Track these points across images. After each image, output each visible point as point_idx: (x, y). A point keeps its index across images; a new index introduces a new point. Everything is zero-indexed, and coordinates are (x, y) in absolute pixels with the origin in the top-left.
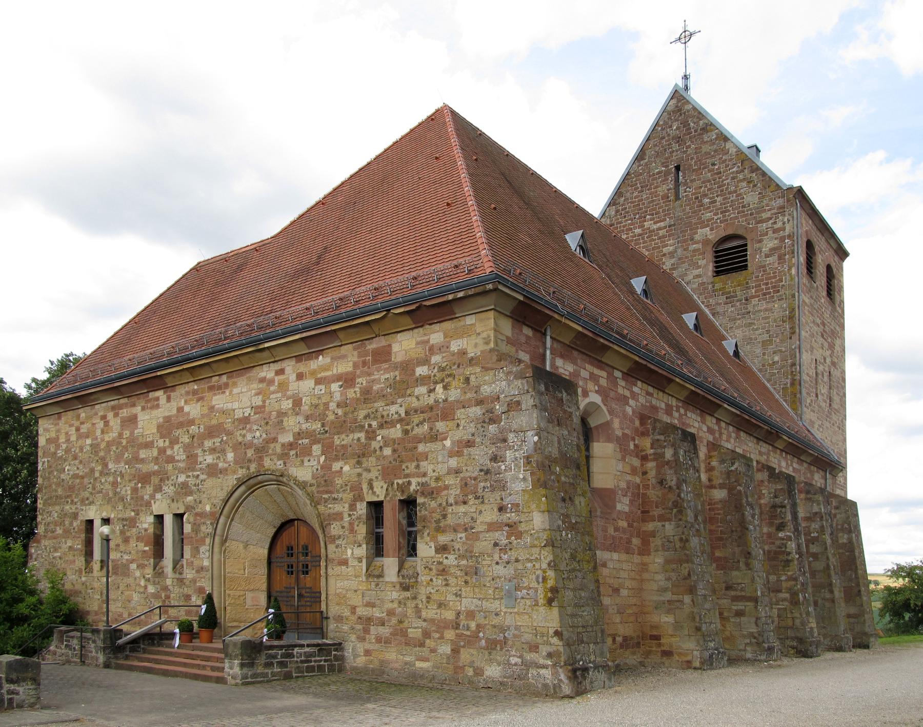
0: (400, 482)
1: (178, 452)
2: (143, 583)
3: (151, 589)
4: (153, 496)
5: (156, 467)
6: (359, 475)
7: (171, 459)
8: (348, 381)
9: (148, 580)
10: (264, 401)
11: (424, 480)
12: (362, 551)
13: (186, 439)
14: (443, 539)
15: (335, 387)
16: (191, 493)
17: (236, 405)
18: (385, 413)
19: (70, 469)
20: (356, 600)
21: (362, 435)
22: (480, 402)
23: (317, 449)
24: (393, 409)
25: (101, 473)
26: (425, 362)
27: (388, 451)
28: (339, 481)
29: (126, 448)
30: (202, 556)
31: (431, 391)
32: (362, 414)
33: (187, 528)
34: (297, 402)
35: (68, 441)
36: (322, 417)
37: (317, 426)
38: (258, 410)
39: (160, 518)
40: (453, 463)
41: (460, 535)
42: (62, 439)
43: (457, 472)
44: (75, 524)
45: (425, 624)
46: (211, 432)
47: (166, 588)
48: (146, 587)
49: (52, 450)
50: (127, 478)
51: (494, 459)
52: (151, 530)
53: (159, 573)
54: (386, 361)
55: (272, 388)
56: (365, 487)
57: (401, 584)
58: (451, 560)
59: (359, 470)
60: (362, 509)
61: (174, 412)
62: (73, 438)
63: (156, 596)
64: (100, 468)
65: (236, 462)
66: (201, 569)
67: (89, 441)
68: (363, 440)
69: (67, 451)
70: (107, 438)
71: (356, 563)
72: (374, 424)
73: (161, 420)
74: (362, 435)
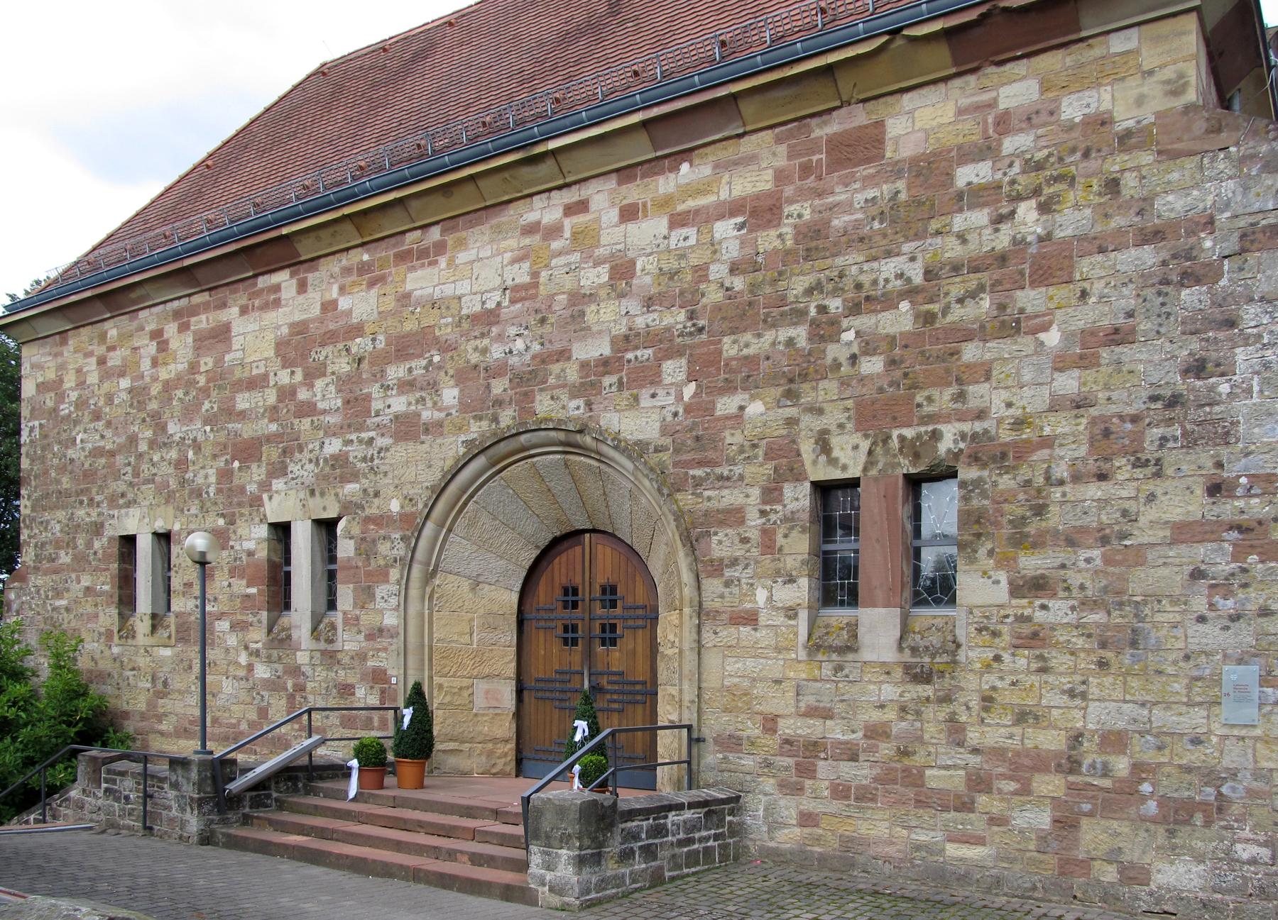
0: (909, 433)
1: (326, 395)
2: (243, 659)
3: (262, 672)
4: (265, 486)
5: (273, 427)
6: (791, 422)
7: (308, 409)
8: (761, 212)
9: (257, 653)
10: (535, 275)
11: (978, 426)
12: (802, 591)
13: (343, 366)
14: (1031, 563)
15: (725, 229)
16: (355, 477)
17: (463, 287)
18: (865, 279)
19: (86, 438)
20: (781, 702)
21: (800, 334)
22: (1152, 236)
23: (674, 370)
24: (888, 268)
25: (152, 444)
26: (986, 150)
27: (873, 366)
28: (733, 438)
29: (206, 391)
30: (380, 604)
31: (999, 220)
32: (798, 285)
33: (345, 548)
34: (622, 270)
35: (81, 384)
36: (689, 300)
37: (677, 318)
38: (519, 293)
39: (282, 531)
40: (1068, 383)
41: (1083, 554)
42: (70, 381)
43: (1080, 404)
44: (97, 545)
45: (975, 760)
46: (403, 348)
47: (296, 671)
48: (250, 668)
49: (50, 404)
50: (208, 450)
51: (1198, 368)
52: (262, 554)
53: (280, 641)
54: (868, 160)
55: (556, 245)
56: (807, 448)
57: (907, 668)
58: (1058, 611)
59: (791, 412)
60: (798, 498)
61: (316, 311)
62: (93, 379)
63: (274, 685)
64: (149, 434)
65: (464, 407)
66: (377, 633)
67: (125, 383)
68: (802, 343)
69: (81, 404)
70: (164, 374)
71: (780, 620)
72: (835, 305)
73: (285, 330)
74: (800, 334)
